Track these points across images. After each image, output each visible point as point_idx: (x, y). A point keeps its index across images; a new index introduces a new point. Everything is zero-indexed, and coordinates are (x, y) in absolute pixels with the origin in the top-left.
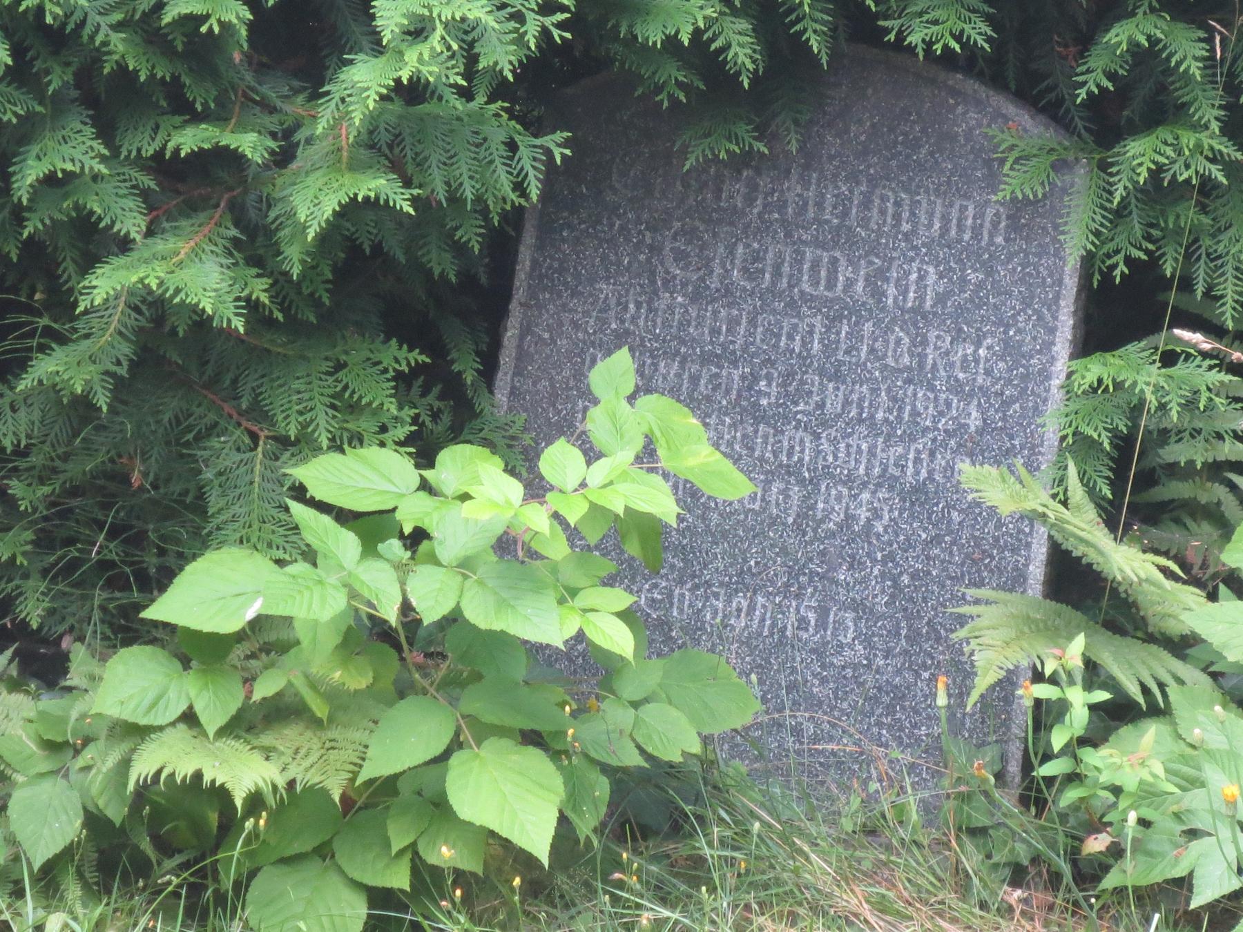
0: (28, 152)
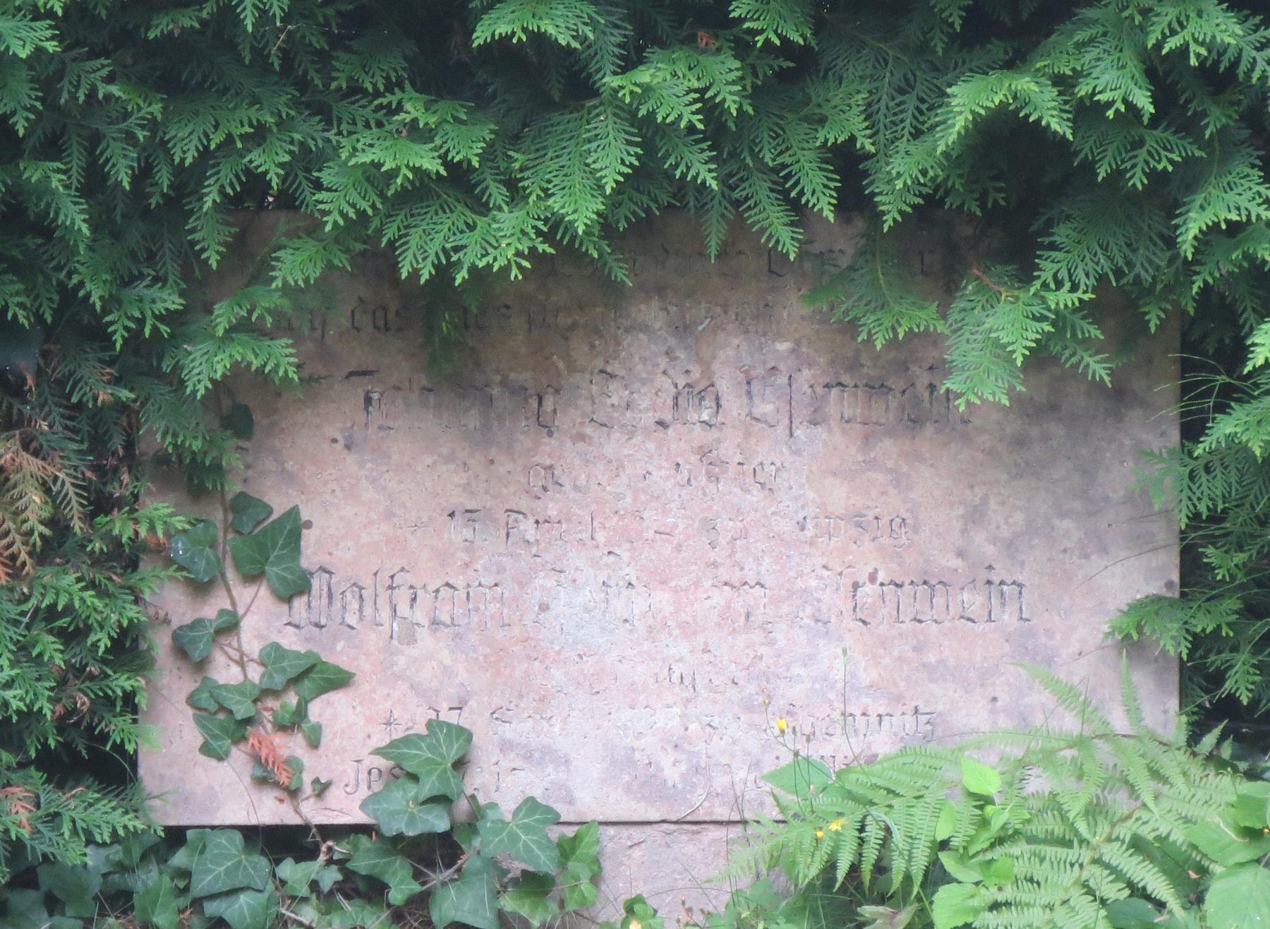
0: (1194, 201)
